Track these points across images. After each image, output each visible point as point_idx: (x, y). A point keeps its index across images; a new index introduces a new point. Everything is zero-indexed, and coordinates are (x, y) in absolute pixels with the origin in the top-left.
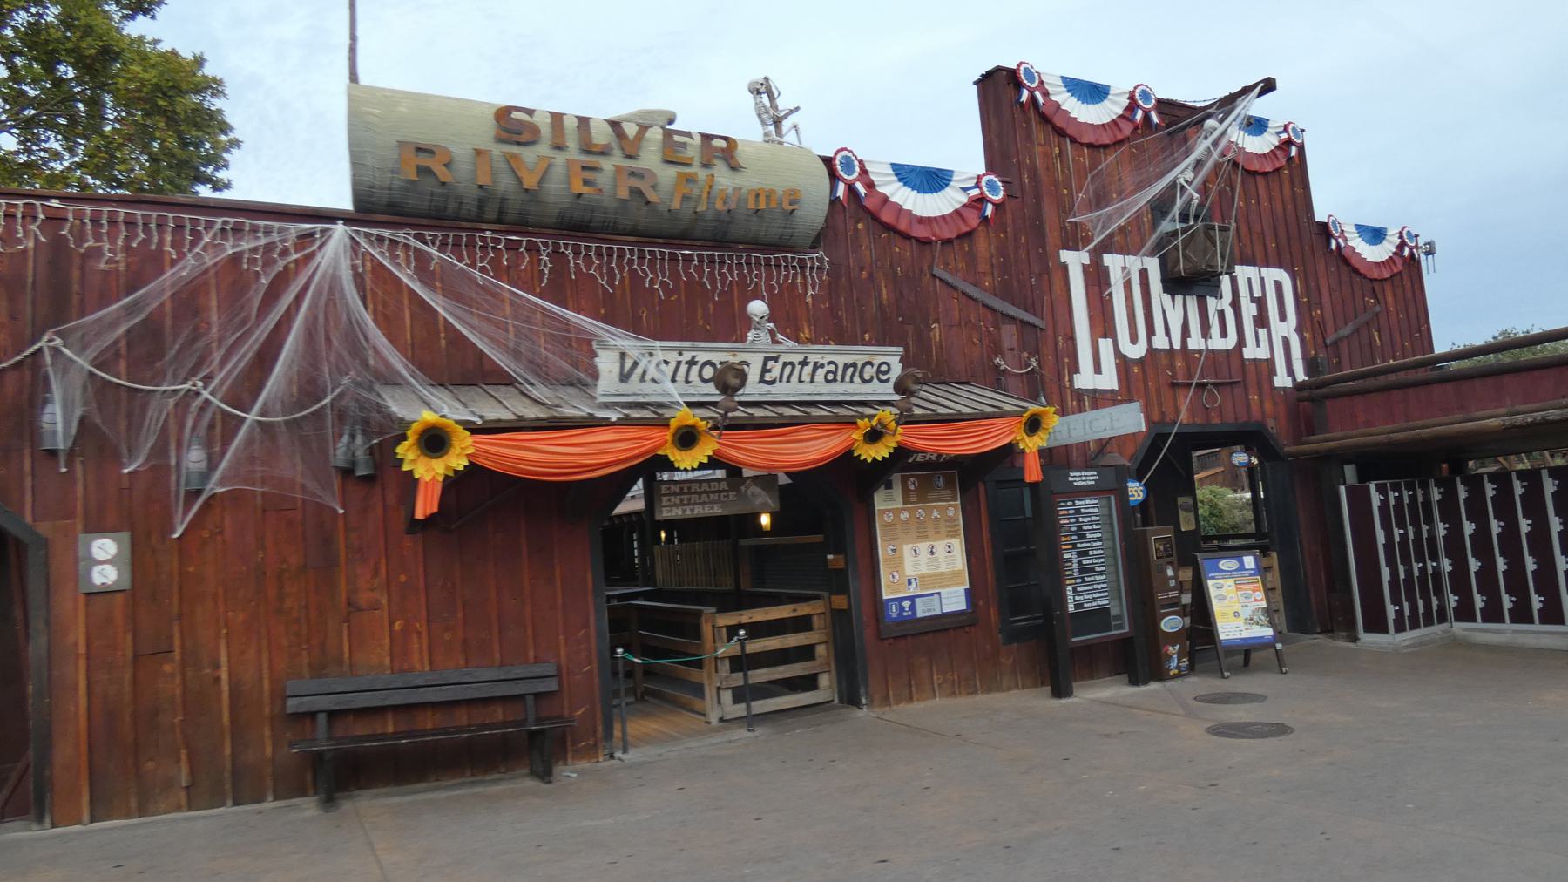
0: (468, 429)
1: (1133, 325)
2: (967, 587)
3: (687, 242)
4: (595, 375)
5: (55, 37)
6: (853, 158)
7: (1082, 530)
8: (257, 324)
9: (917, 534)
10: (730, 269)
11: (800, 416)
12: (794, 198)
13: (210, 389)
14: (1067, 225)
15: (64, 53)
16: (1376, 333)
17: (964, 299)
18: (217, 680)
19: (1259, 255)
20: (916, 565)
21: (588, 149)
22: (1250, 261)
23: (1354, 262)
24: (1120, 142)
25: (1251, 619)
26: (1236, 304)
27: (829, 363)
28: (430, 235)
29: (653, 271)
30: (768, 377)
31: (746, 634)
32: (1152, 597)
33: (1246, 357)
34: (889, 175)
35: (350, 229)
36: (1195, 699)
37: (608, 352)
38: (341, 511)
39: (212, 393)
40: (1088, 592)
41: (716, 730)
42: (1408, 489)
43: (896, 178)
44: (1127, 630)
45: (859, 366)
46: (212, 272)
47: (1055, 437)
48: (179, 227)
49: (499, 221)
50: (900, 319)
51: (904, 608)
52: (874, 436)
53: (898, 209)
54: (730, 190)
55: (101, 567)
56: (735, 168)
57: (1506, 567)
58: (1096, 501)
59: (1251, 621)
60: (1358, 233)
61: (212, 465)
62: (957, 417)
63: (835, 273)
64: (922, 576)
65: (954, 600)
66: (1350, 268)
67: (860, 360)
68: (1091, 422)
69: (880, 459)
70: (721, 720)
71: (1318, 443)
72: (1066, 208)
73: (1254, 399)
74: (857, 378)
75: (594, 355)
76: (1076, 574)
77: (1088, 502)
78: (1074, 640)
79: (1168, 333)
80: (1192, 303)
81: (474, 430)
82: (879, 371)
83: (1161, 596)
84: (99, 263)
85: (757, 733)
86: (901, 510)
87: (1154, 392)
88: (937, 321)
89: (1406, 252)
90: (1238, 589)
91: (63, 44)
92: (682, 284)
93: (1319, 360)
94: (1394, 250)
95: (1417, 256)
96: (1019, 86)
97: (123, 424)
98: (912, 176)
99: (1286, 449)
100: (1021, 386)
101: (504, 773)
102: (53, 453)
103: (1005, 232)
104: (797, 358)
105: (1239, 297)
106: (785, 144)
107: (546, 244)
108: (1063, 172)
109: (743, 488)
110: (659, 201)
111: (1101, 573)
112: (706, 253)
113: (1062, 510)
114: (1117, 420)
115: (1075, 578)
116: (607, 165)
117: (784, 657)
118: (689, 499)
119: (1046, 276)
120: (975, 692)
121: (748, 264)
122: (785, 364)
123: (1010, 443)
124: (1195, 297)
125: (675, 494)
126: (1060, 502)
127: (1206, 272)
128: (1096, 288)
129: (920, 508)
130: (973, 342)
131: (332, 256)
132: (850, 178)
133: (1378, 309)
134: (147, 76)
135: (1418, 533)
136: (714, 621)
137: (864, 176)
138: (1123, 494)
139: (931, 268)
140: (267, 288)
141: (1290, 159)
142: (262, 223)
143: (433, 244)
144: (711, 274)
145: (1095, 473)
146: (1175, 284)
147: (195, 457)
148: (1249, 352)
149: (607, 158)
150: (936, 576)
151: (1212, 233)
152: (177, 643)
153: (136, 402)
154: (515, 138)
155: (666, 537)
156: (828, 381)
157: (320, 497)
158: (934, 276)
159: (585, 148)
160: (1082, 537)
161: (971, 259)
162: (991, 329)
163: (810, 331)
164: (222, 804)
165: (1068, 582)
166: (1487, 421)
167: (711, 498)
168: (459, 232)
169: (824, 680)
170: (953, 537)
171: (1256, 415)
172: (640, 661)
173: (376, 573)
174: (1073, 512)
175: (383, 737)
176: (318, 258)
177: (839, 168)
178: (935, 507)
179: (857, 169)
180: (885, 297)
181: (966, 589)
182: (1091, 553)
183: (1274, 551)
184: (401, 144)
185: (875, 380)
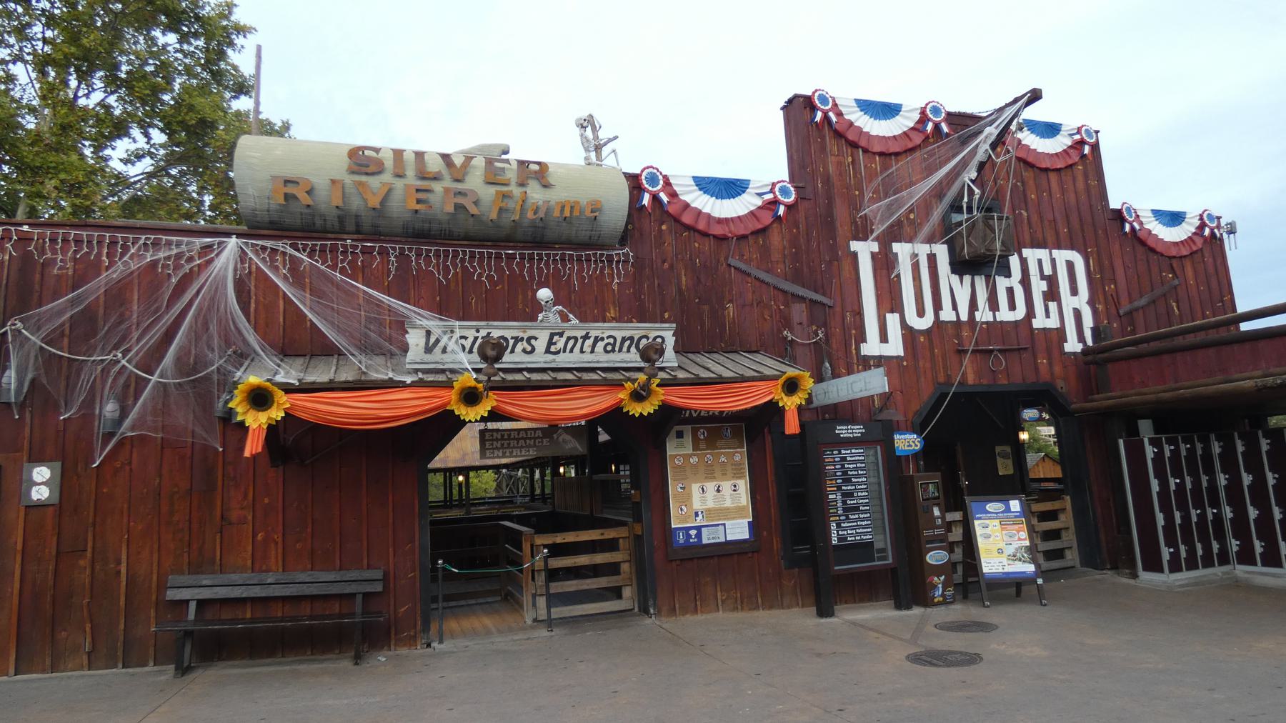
0: (282, 390)
1: (920, 301)
2: (751, 520)
3: (511, 244)
4: (405, 349)
5: (170, 113)
6: (658, 174)
9: (706, 475)
10: (547, 264)
11: (577, 380)
12: (596, 208)
13: (126, 359)
15: (175, 124)
16: (1174, 304)
17: (758, 283)
18: (119, 572)
19: (1050, 239)
20: (704, 500)
21: (423, 175)
23: (1151, 243)
24: (912, 150)
25: (1014, 556)
26: (1026, 282)
27: (608, 337)
28: (302, 244)
29: (481, 267)
30: (553, 349)
31: (549, 552)
32: (919, 534)
33: (1035, 326)
34: (1150, 217)
35: (240, 241)
36: (936, 626)
37: (415, 330)
38: (221, 449)
39: (127, 361)
41: (532, 628)
42: (1185, 442)
44: (890, 561)
46: (136, 274)
47: (829, 396)
48: (113, 243)
49: (358, 232)
50: (697, 301)
52: (638, 397)
54: (540, 203)
55: (38, 487)
56: (546, 186)
57: (1281, 516)
58: (862, 451)
59: (1014, 557)
60: (1155, 217)
61: (124, 413)
62: (718, 380)
63: (639, 264)
64: (709, 510)
65: (739, 530)
66: (1147, 248)
67: (637, 336)
68: (852, 384)
69: (645, 414)
70: (535, 620)
71: (1103, 401)
72: (855, 205)
73: (1042, 363)
74: (633, 349)
76: (840, 512)
77: (853, 451)
78: (836, 568)
79: (955, 307)
80: (980, 282)
81: (288, 389)
83: (926, 533)
84: (54, 269)
85: (553, 633)
86: (691, 456)
87: (940, 358)
88: (731, 301)
89: (1207, 232)
90: (1002, 529)
91: (175, 117)
92: (506, 277)
93: (1101, 329)
94: (1194, 231)
95: (1218, 235)
96: (814, 108)
97: (63, 384)
98: (712, 186)
99: (1073, 406)
100: (809, 354)
101: (337, 654)
102: (8, 404)
103: (798, 228)
104: (579, 334)
105: (1029, 275)
106: (603, 166)
107: (394, 249)
108: (855, 176)
109: (555, 436)
110: (479, 213)
111: (865, 512)
113: (828, 458)
114: (869, 382)
115: (840, 516)
116: (438, 187)
117: (595, 571)
118: (509, 444)
119: (836, 262)
120: (757, 608)
121: (563, 260)
122: (569, 339)
123: (770, 401)
124: (983, 277)
125: (497, 440)
127: (985, 256)
128: (884, 272)
129: (708, 454)
130: (764, 318)
131: (225, 261)
132: (655, 189)
133: (1176, 282)
134: (228, 137)
135: (1197, 483)
136: (533, 540)
137: (668, 188)
138: (889, 446)
139: (726, 259)
140: (176, 285)
141: (1083, 156)
142: (174, 239)
143: (304, 251)
144: (531, 268)
145: (862, 427)
146: (961, 266)
147: (111, 408)
148: (1039, 323)
149: (439, 182)
150: (721, 510)
151: (991, 222)
152: (90, 544)
153: (74, 369)
154: (364, 169)
155: (615, 469)
156: (606, 351)
157: (205, 440)
158: (729, 265)
159: (420, 176)
160: (847, 481)
161: (765, 252)
162: (782, 307)
163: (615, 310)
164: (115, 666)
165: (831, 519)
166: (1243, 382)
167: (527, 444)
168: (326, 241)
169: (627, 592)
170: (740, 478)
171: (1044, 374)
172: (457, 571)
173: (245, 497)
174: (839, 459)
175: (243, 621)
177: (644, 182)
178: (722, 453)
179: (661, 182)
180: (684, 282)
181: (749, 522)
182: (855, 494)
183: (1067, 495)
184: (274, 178)
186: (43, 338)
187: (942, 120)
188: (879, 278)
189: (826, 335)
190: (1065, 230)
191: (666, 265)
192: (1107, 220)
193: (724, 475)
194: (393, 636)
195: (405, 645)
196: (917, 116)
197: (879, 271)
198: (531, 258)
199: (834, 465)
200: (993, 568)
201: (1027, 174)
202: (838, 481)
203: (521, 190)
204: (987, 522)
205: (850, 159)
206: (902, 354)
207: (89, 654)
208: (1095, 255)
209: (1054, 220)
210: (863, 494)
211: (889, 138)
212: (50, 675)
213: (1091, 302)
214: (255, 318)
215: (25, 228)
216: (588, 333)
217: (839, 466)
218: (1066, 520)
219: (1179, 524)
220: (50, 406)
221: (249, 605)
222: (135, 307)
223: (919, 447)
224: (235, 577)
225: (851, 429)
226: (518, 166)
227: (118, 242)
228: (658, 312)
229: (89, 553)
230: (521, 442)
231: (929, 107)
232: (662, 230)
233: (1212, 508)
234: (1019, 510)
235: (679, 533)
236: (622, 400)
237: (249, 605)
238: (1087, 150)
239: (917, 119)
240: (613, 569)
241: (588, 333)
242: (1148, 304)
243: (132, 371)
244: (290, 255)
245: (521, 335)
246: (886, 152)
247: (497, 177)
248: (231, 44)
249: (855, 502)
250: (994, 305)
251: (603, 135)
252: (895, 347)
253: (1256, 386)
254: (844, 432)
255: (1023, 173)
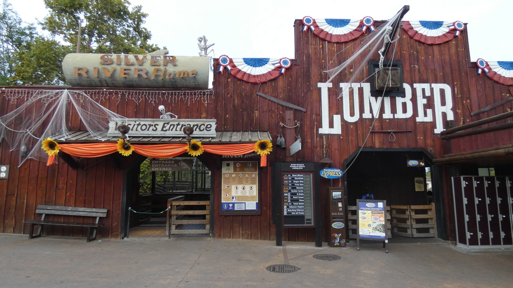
1: (352, 109)
3: (164, 89)
4: (108, 128)
7: (295, 186)
8: (44, 115)
14: (323, 73)
18: (24, 203)
20: (237, 192)
22: (422, 81)
23: (496, 78)
26: (414, 100)
30: (164, 129)
33: (417, 121)
34: (497, 65)
38: (57, 163)
39: (30, 132)
40: (294, 209)
43: (244, 63)
44: (313, 224)
45: (199, 126)
46: (35, 102)
48: (28, 93)
49: (108, 86)
51: (230, 206)
53: (500, 76)
54: (172, 72)
55: (2, 173)
58: (303, 175)
59: (376, 229)
62: (229, 143)
64: (239, 196)
71: (447, 157)
74: (198, 130)
75: (109, 122)
76: (289, 201)
77: (298, 175)
78: (285, 225)
79: (371, 111)
80: (387, 101)
82: (207, 127)
83: (333, 214)
86: (232, 174)
88: (257, 110)
92: (162, 101)
96: (303, 25)
98: (251, 62)
107: (120, 92)
109: (179, 163)
111: (302, 202)
112: (170, 92)
113: (285, 178)
115: (289, 203)
116: (132, 68)
118: (161, 166)
121: (184, 94)
124: (389, 98)
125: (156, 164)
126: (285, 175)
128: (334, 96)
130: (272, 117)
132: (225, 64)
139: (256, 92)
142: (47, 91)
145: (304, 165)
146: (376, 93)
148: (420, 118)
153: (14, 134)
160: (294, 188)
161: (275, 89)
162: (281, 112)
165: (284, 204)
173: (64, 180)
174: (291, 178)
175: (60, 223)
176: (60, 99)
177: (220, 62)
179: (228, 61)
182: (297, 194)
184: (75, 68)
185: (205, 130)
186: (7, 124)
187: (371, 25)
188: (331, 100)
189: (301, 124)
190: (441, 74)
191: (229, 96)
192: (468, 68)
193: (247, 183)
194: (110, 234)
195: (114, 237)
196: (358, 24)
197: (331, 96)
198: (172, 94)
199: (288, 181)
200: (365, 233)
201: (420, 47)
202: (289, 188)
203: (165, 67)
204: (366, 211)
205: (321, 46)
206: (340, 133)
207: (14, 228)
208: (458, 86)
209: (434, 69)
210: (302, 194)
211: (436, 37)
212: (2, 234)
213: (454, 109)
214: (71, 117)
215: (4, 89)
216: (179, 123)
217: (291, 182)
218: (432, 214)
219: (479, 221)
220: (8, 147)
221: (63, 217)
222: (34, 114)
223: (340, 175)
224: (58, 207)
225: (298, 166)
226: (164, 58)
227: (30, 93)
228: (223, 115)
229: (15, 196)
230: (166, 165)
231: (305, 19)
232: (228, 81)
233: (503, 215)
234: (382, 207)
235: (225, 205)
236: (187, 150)
237: (63, 217)
238: (458, 33)
239: (358, 25)
240: (203, 217)
241: (179, 123)
242: (491, 110)
243: (31, 136)
244: (84, 96)
245: (152, 123)
246: (340, 42)
247: (156, 63)
248: (141, 21)
249: (297, 197)
250: (394, 110)
251: (208, 44)
252: (337, 130)
253: (505, 152)
254: (294, 167)
255: (418, 47)
